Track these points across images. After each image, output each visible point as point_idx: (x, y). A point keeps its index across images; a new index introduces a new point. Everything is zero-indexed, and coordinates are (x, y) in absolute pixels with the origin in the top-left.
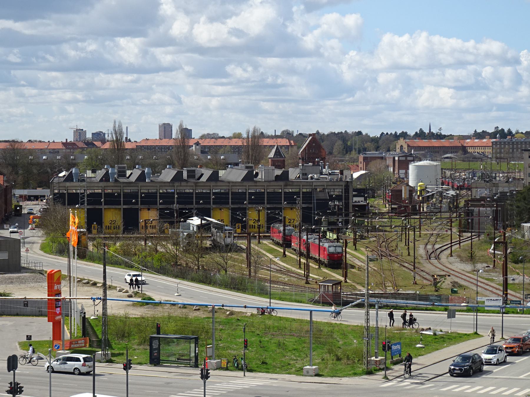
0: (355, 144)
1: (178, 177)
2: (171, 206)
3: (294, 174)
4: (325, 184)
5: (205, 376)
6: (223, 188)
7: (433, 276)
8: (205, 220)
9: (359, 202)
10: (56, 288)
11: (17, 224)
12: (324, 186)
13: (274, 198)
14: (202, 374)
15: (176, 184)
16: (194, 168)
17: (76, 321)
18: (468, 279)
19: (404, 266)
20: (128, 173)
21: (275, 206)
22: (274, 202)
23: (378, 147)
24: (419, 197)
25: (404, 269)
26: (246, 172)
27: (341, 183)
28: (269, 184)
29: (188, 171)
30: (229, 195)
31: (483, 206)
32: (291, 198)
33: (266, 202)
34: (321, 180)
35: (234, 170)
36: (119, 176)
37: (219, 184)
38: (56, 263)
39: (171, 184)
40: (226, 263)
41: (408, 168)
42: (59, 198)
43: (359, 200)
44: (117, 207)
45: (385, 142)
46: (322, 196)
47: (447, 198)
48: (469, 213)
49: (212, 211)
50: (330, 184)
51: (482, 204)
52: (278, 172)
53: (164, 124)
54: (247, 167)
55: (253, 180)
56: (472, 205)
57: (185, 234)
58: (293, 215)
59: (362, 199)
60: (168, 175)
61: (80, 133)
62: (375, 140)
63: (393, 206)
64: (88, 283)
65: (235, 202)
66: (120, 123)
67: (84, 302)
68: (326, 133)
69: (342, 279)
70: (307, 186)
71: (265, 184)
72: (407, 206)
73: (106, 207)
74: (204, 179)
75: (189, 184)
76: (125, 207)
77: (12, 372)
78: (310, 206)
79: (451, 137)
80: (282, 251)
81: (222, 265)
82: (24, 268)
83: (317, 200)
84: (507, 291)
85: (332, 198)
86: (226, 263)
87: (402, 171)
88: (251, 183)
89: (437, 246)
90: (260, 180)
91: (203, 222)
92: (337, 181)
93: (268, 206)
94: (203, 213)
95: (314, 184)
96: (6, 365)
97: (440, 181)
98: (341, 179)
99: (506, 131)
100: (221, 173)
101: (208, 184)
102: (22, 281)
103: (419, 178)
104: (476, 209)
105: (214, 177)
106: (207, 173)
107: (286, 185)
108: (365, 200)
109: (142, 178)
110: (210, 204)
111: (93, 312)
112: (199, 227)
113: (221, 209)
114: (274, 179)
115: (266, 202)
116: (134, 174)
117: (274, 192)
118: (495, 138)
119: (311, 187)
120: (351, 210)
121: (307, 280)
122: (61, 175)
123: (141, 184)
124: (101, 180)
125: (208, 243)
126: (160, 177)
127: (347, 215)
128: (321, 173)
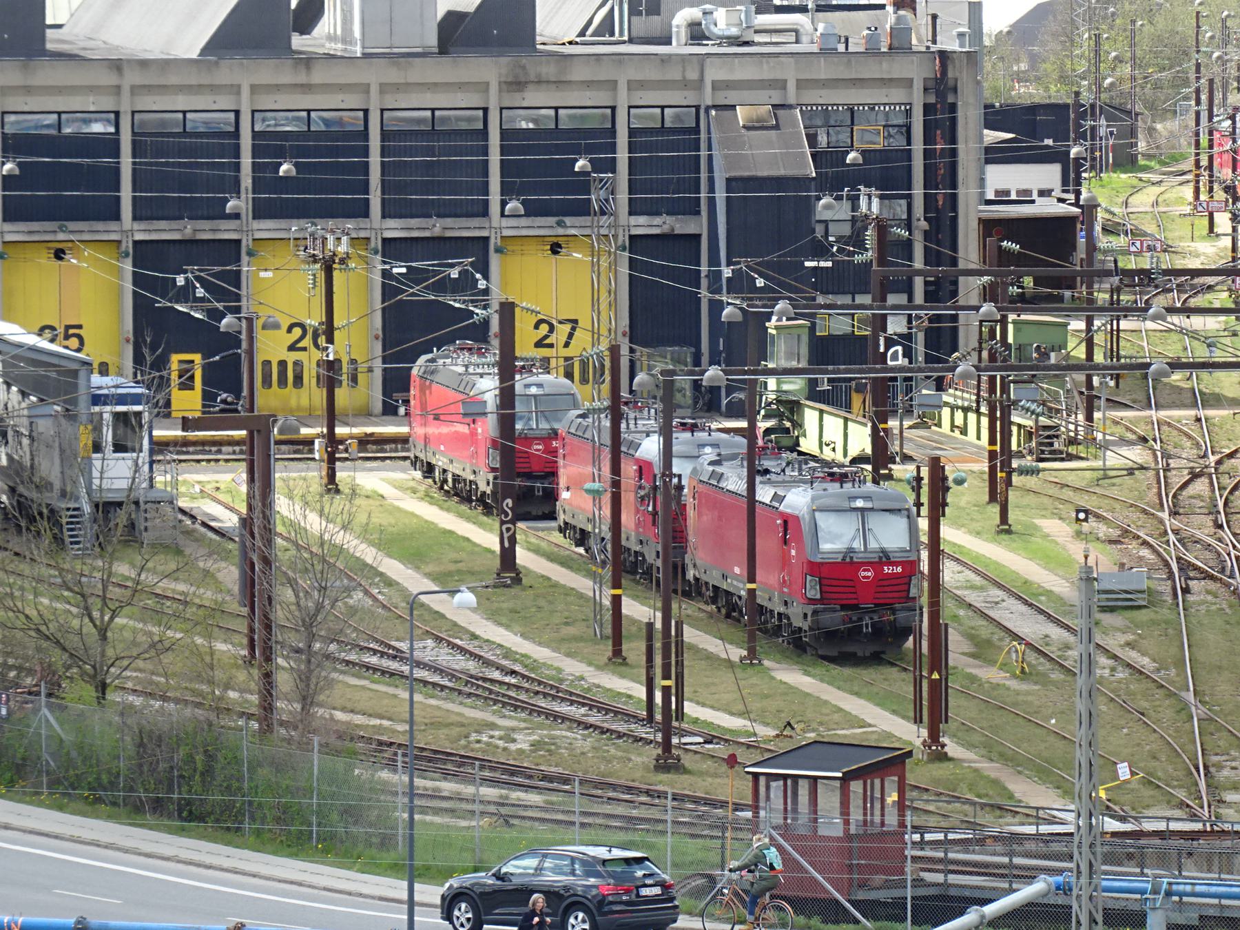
9: (1025, 198)
12: (781, 85)
21: (437, 227)
28: (393, 75)
32: (551, 172)
37: (46, 74)
46: (786, 156)
50: (823, 71)
58: (563, 288)
59: (1049, 175)
69: (911, 734)
71: (373, 76)
81: (73, 641)
83: (731, 183)
86: (103, 633)
88: (267, 71)
90: (336, 48)
92: (872, 52)
93: (395, 229)
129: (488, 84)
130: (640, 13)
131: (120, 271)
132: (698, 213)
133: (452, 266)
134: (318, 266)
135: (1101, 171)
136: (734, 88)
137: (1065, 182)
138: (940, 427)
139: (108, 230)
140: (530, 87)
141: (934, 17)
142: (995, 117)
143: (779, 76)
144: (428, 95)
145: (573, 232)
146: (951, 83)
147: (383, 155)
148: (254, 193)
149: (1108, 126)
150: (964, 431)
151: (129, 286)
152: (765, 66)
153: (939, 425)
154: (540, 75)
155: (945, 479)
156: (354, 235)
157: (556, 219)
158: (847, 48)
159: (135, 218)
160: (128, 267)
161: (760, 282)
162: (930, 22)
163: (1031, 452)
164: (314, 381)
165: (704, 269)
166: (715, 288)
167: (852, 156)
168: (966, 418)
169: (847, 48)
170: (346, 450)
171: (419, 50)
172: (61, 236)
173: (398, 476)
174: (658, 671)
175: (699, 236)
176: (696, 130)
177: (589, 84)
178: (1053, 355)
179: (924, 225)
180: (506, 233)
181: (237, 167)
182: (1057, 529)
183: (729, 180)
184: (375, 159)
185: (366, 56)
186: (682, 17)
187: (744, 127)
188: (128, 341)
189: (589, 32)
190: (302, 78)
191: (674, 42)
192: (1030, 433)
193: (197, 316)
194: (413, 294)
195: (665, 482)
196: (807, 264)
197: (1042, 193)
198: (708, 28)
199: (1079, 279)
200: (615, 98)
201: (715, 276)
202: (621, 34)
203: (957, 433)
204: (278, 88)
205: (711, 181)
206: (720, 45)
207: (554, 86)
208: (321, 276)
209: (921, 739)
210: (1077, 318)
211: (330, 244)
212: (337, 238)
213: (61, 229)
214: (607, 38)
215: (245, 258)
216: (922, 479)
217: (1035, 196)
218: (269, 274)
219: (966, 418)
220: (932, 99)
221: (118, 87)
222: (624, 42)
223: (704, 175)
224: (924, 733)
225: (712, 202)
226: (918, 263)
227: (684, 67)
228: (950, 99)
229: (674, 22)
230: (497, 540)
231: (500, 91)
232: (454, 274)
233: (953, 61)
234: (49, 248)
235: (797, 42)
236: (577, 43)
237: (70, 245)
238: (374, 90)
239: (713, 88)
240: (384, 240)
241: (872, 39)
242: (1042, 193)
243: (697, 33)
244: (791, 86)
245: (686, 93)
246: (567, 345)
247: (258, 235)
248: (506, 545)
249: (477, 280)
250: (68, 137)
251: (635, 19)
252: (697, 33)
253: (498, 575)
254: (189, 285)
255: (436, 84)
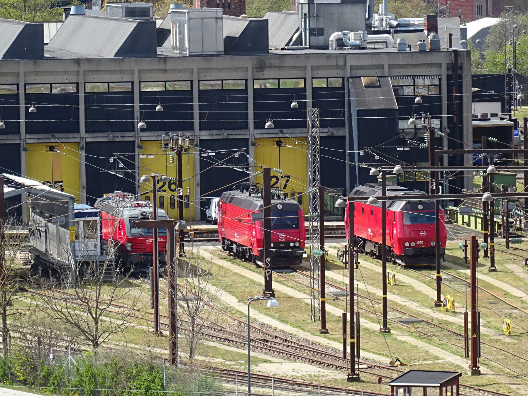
4: (386, 62)
6: (59, 79)
9: (484, 117)
11: (7, 189)
12: (382, 67)
13: (223, 109)
21: (225, 134)
26: (129, 27)
27: (436, 59)
28: (203, 64)
30: (132, 101)
32: (280, 109)
33: (196, 120)
34: (370, 49)
35: (91, 22)
40: (96, 320)
46: (383, 100)
49: (23, 154)
50: (401, 60)
52: (234, 26)
54: (131, 13)
55: (154, 54)
59: (495, 107)
70: (328, 68)
71: (195, 65)
78: (340, 132)
81: (83, 325)
83: (360, 113)
86: (96, 320)
88: (146, 63)
90: (177, 53)
92: (422, 51)
93: (205, 135)
95: (350, 62)
100: (50, 31)
107: (261, 67)
110: (18, 132)
113: (279, 143)
114: (221, 48)
115: (196, 120)
119: (340, 73)
121: (353, 369)
127: (456, 160)
128: (369, 29)
129: (193, 69)
130: (314, 35)
131: (80, 156)
132: (344, 126)
133: (236, 152)
134: (175, 152)
135: (517, 105)
136: (361, 69)
137: (503, 110)
138: (457, 223)
139: (74, 138)
140: (267, 69)
141: (451, 35)
142: (477, 80)
143: (381, 63)
144: (415, 69)
145: (287, 135)
146: (459, 65)
147: (199, 102)
149: (519, 85)
150: (469, 225)
151: (84, 162)
152: (374, 59)
153: (457, 222)
154: (271, 63)
155: (478, 246)
156: (191, 138)
157: (279, 129)
158: (410, 50)
159: (86, 132)
160: (83, 153)
161: (377, 158)
162: (448, 38)
163: (501, 234)
164: (169, 205)
165: (347, 151)
166: (352, 159)
167: (417, 99)
168: (469, 219)
169: (410, 50)
170: (189, 237)
171: (215, 53)
172: (53, 140)
173: (211, 248)
174: (349, 337)
175: (344, 137)
176: (343, 88)
177: (293, 68)
178: (509, 189)
179: (448, 131)
180: (256, 136)
181: (133, 107)
183: (358, 111)
184: (196, 104)
185: (191, 56)
186: (333, 37)
187: (365, 87)
188: (84, 188)
189: (291, 44)
190: (162, 66)
191: (330, 49)
192: (500, 225)
193: (120, 176)
194: (218, 165)
195: (350, 248)
196: (398, 149)
197: (492, 116)
198: (346, 42)
199: (513, 154)
200: (305, 74)
201: (352, 155)
202: (306, 44)
203: (465, 226)
204: (151, 71)
205: (350, 111)
206: (351, 49)
207: (277, 69)
208: (176, 157)
209: (468, 365)
210: (520, 172)
211: (180, 142)
212: (183, 140)
213: (53, 137)
214: (299, 47)
215: (137, 149)
216: (467, 246)
217: (489, 117)
218: (152, 157)
219: (469, 219)
220: (451, 73)
221: (78, 71)
222: (307, 48)
223: (346, 109)
224: (470, 362)
225: (350, 121)
226: (445, 149)
227: (337, 59)
228: (459, 73)
229: (331, 39)
230: (264, 278)
231: (253, 71)
232: (237, 155)
233: (460, 55)
234: (47, 146)
235: (387, 48)
236: (285, 49)
237: (57, 144)
238: (195, 71)
239: (351, 69)
240: (201, 140)
241: (422, 46)
242: (492, 116)
243: (341, 43)
244: (386, 68)
245: (338, 71)
246: (285, 187)
247: (143, 139)
248: (268, 279)
249: (248, 158)
250: (55, 94)
251: (312, 38)
252: (341, 43)
253: (264, 292)
254: (115, 162)
255: (223, 68)
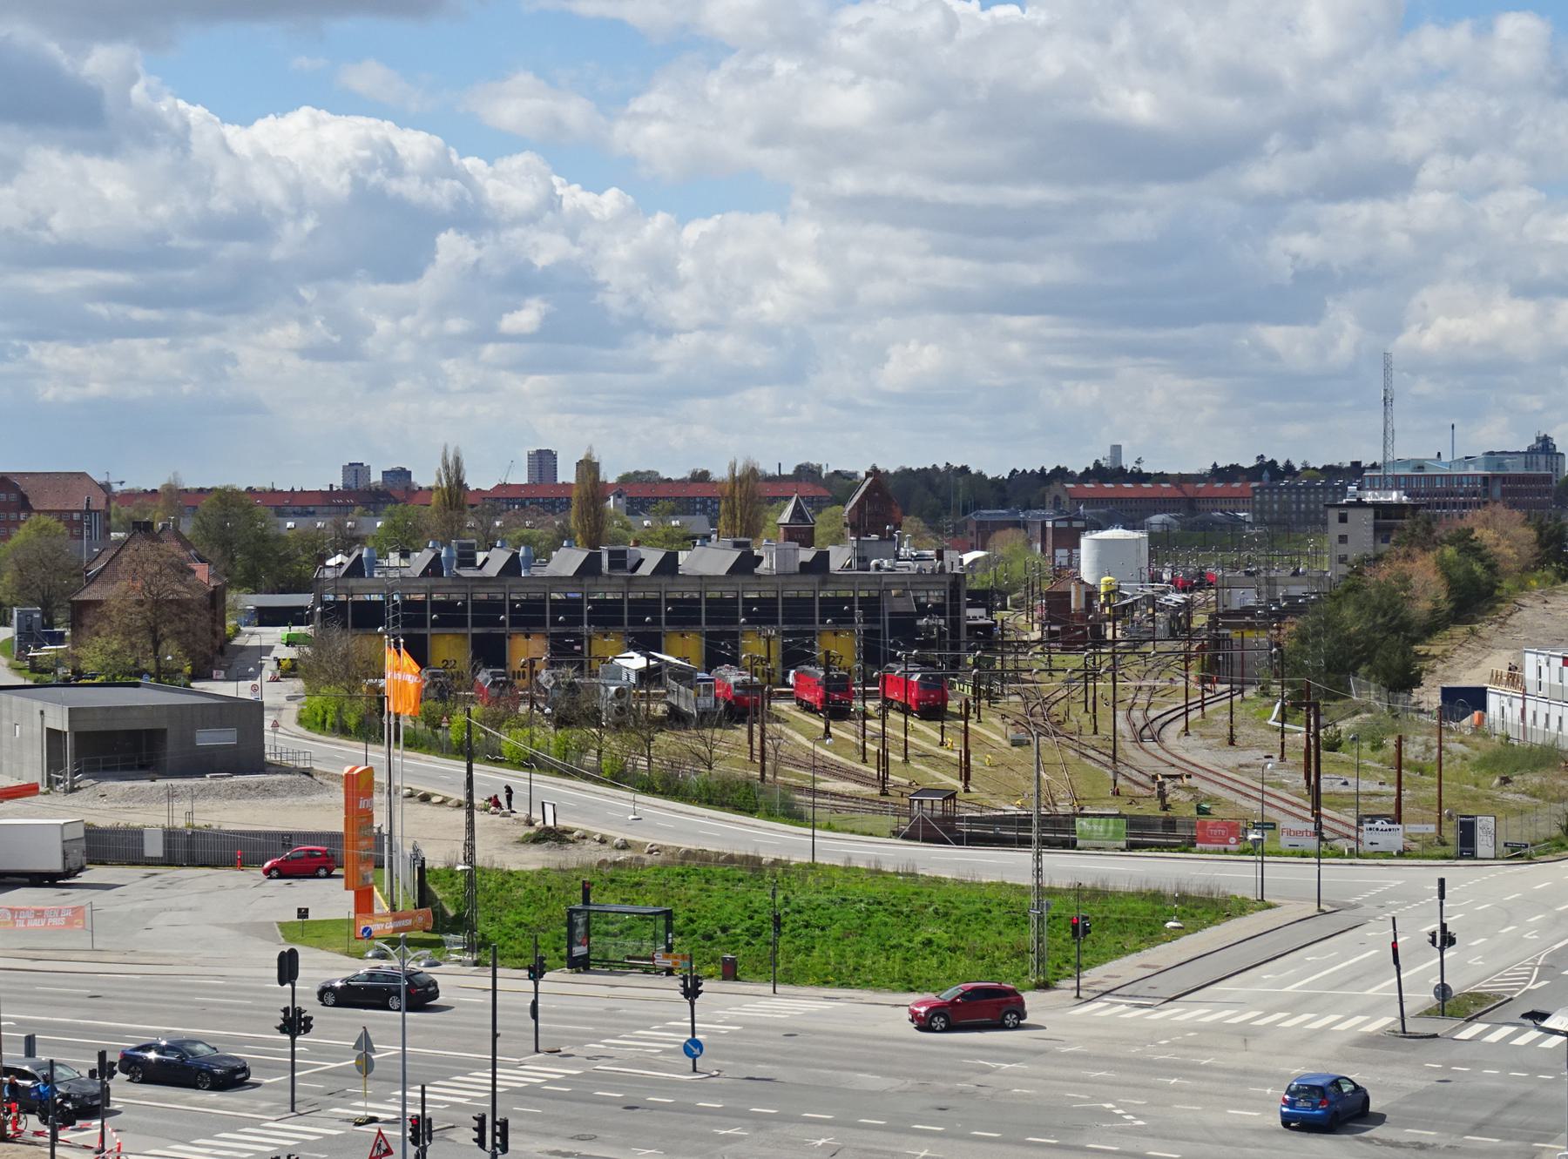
0: (956, 494)
1: (589, 568)
2: (578, 630)
3: (840, 557)
5: (691, 993)
7: (1155, 778)
8: (654, 658)
9: (975, 618)
10: (362, 805)
13: (798, 610)
14: (685, 986)
15: (587, 581)
16: (622, 547)
17: (405, 876)
18: (1230, 783)
19: (1088, 757)
20: (480, 557)
22: (798, 616)
23: (1005, 500)
24: (1103, 606)
25: (1088, 762)
26: (736, 554)
29: (611, 553)
31: (1250, 626)
32: (837, 611)
36: (461, 564)
37: (679, 580)
38: (348, 755)
39: (576, 582)
41: (1078, 546)
42: (335, 614)
43: (975, 615)
44: (458, 631)
45: (1027, 490)
46: (902, 606)
47: (1163, 608)
48: (1218, 642)
50: (919, 579)
51: (1248, 624)
52: (806, 555)
53: (539, 452)
54: (737, 545)
55: (752, 573)
56: (1225, 626)
57: (613, 689)
58: (843, 647)
59: (982, 612)
60: (567, 561)
61: (356, 470)
62: (997, 483)
63: (1054, 628)
64: (411, 796)
65: (716, 619)
66: (457, 450)
67: (429, 835)
68: (892, 471)
69: (960, 785)
72: (1074, 625)
73: (434, 631)
74: (645, 570)
75: (614, 581)
76: (476, 631)
77: (288, 986)
79: (1162, 477)
80: (822, 726)
82: (270, 764)
83: (891, 614)
84: (1318, 809)
85: (923, 610)
87: (1062, 553)
88: (747, 579)
89: (1153, 714)
91: (652, 663)
93: (786, 628)
94: (646, 644)
95: (885, 580)
96: (275, 972)
97: (1146, 577)
98: (942, 568)
99: (1281, 464)
100: (683, 556)
101: (656, 580)
102: (266, 791)
103: (1102, 567)
104: (1235, 635)
105: (668, 565)
106: (652, 558)
107: (824, 583)
108: (989, 614)
109: (512, 567)
111: (442, 852)
112: (642, 675)
116: (493, 561)
117: (798, 598)
118: (1259, 479)
120: (964, 636)
122: (331, 562)
123: (511, 581)
124: (424, 573)
125: (660, 709)
126: (550, 566)
128: (897, 557)
148: (465, 625)
182: (996, 721)
186: (873, 562)
243: (878, 567)
